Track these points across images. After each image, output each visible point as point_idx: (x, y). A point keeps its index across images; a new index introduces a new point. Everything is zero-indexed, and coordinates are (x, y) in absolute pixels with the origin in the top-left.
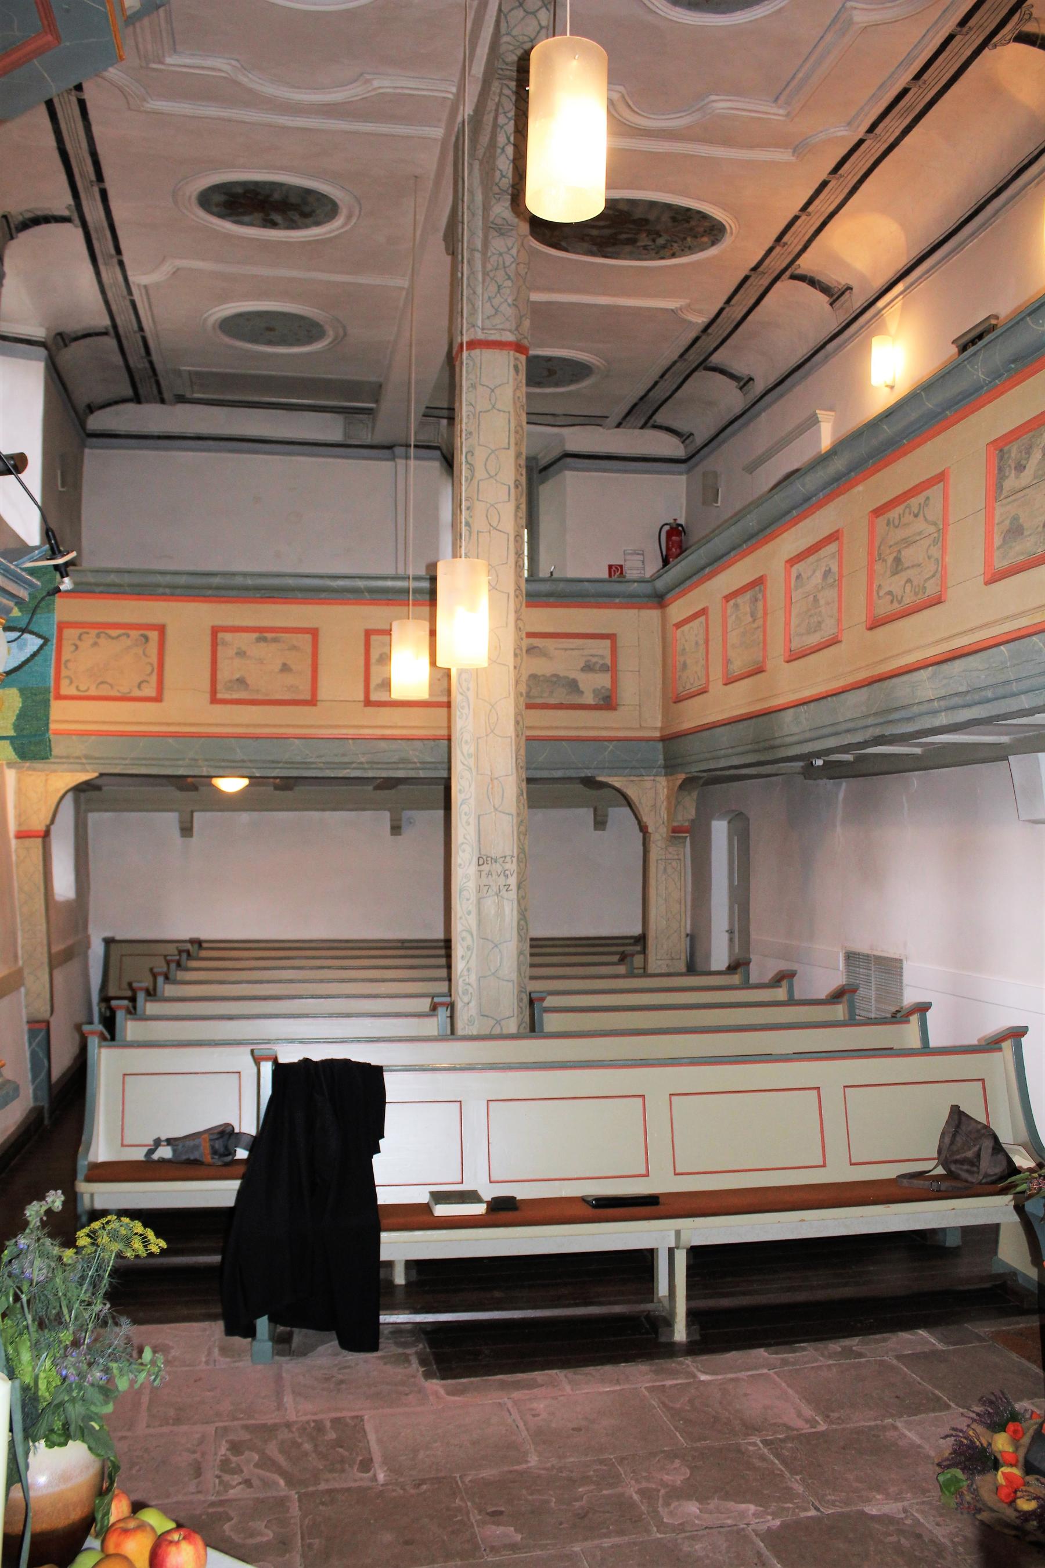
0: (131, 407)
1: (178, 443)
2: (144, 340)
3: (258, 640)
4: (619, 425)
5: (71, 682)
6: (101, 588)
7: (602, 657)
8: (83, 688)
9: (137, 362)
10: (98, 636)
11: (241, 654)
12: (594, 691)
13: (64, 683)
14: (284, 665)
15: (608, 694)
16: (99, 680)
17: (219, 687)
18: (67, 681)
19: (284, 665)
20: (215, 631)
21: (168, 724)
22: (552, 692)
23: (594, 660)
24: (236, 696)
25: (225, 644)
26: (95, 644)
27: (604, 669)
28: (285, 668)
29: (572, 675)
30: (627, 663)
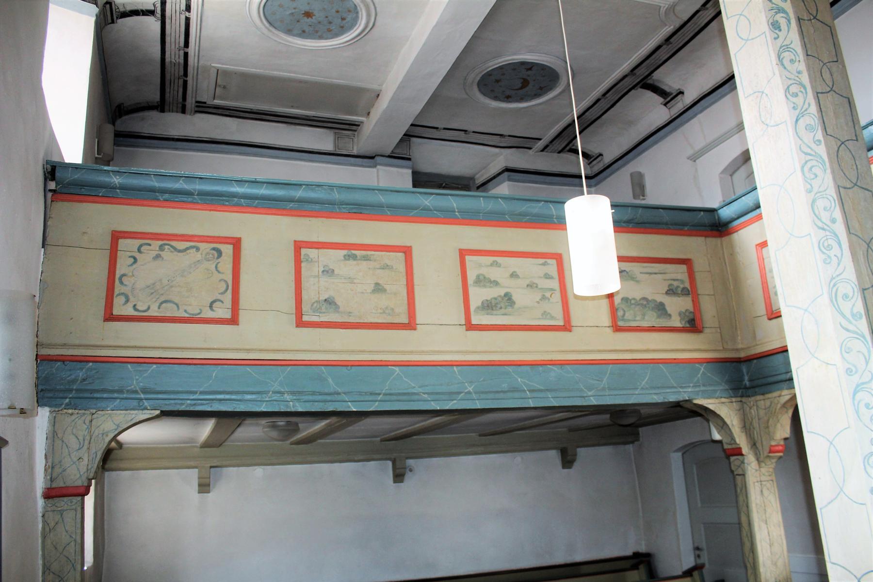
0: (154, 114)
2: (188, 20)
3: (347, 257)
5: (127, 301)
6: (166, 196)
7: (682, 282)
9: (173, 55)
10: (161, 248)
11: (328, 272)
12: (680, 314)
13: (118, 301)
14: (377, 284)
15: (691, 316)
16: (162, 299)
17: (305, 308)
18: (122, 299)
19: (377, 284)
21: (248, 351)
22: (644, 315)
23: (675, 283)
24: (324, 318)
25: (310, 261)
26: (158, 257)
27: (685, 292)
28: (378, 289)
29: (660, 298)
30: (704, 287)
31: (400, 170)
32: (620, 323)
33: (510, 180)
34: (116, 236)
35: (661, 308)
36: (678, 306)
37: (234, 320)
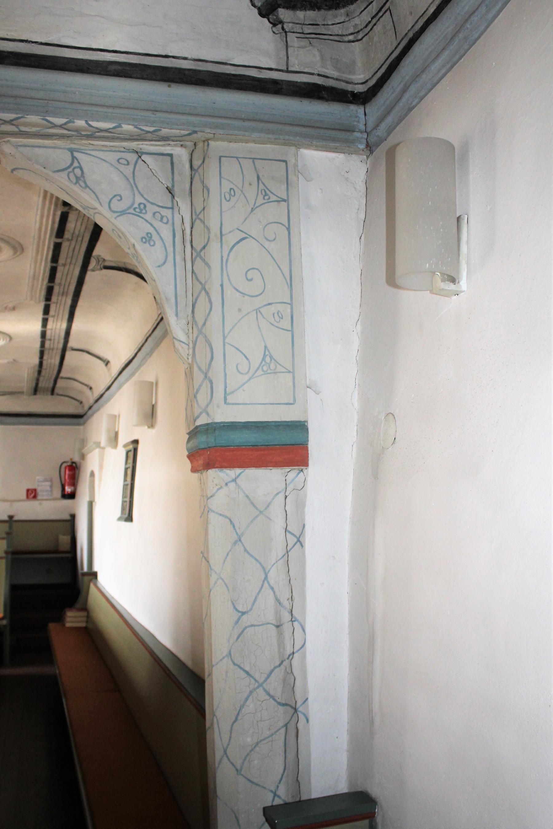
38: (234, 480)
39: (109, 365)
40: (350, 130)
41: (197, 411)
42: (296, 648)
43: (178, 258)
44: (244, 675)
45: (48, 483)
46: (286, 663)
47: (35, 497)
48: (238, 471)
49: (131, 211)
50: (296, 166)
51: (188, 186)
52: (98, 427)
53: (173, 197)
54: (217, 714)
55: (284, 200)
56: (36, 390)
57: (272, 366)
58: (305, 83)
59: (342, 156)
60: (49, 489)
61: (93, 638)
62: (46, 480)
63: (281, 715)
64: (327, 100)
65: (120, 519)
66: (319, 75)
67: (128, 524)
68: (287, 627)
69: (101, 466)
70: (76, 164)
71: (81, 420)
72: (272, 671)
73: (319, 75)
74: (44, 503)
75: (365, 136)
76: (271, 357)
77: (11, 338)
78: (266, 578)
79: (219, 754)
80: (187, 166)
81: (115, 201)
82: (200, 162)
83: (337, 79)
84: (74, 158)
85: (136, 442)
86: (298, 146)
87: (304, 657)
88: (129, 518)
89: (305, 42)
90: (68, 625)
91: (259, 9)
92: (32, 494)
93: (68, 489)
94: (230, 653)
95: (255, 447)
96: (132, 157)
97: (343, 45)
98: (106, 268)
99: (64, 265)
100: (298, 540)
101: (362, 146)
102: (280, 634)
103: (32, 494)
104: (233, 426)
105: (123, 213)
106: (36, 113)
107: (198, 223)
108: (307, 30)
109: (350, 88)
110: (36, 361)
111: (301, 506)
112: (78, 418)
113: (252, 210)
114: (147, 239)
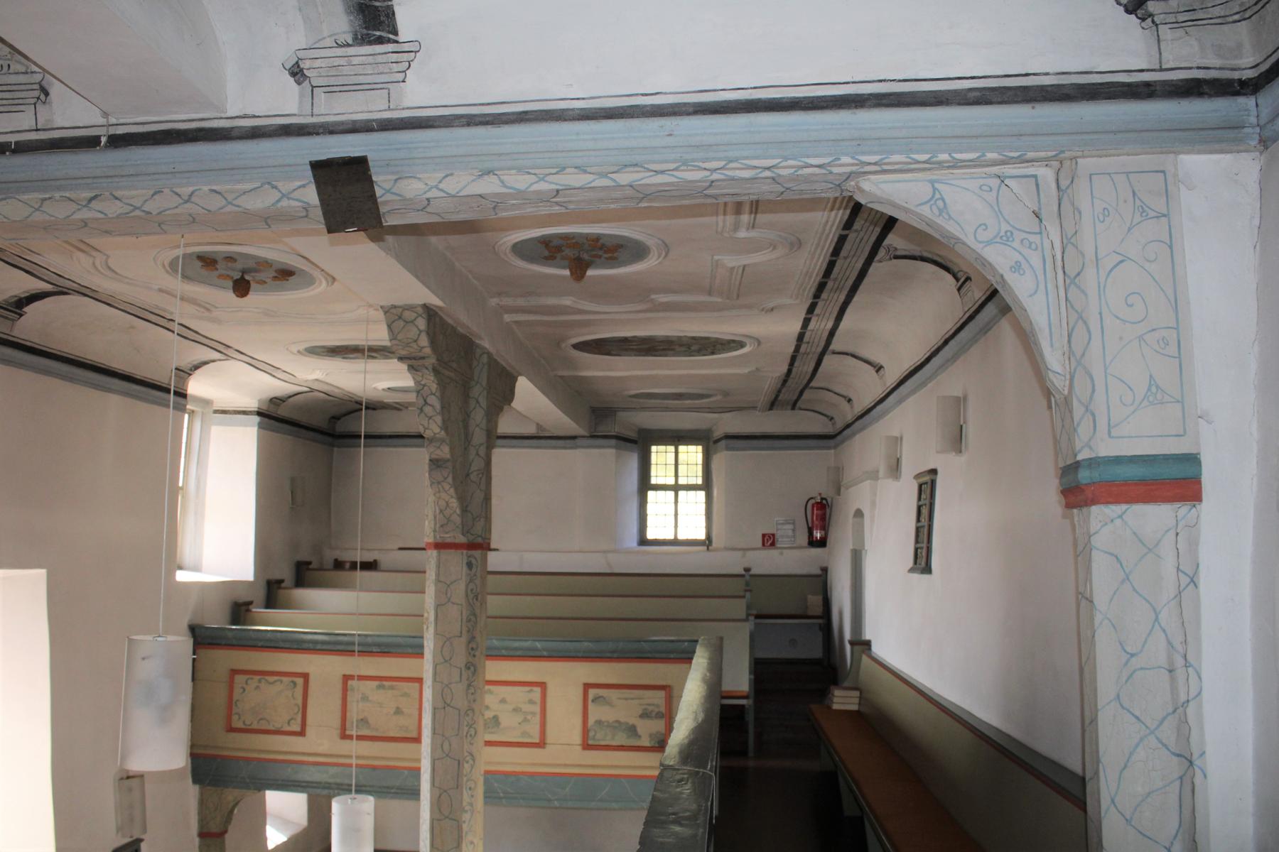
1: (379, 441)
3: (379, 687)
4: (771, 408)
7: (658, 706)
8: (248, 722)
10: (260, 681)
11: (365, 698)
12: (651, 735)
13: (235, 718)
20: (346, 678)
23: (651, 708)
26: (257, 687)
27: (659, 716)
28: (398, 711)
29: (632, 721)
31: (602, 451)
32: (590, 742)
33: (728, 448)
34: (234, 672)
35: (632, 731)
36: (646, 729)
37: (302, 733)
38: (1120, 517)
39: (882, 372)
40: (1238, 127)
41: (1078, 445)
42: (1191, 696)
43: (1049, 286)
44: (1134, 720)
45: (791, 527)
46: (1180, 710)
47: (773, 544)
48: (1124, 507)
49: (998, 240)
50: (1176, 175)
51: (1055, 208)
52: (868, 448)
53: (1041, 220)
54: (1103, 760)
55: (1164, 216)
56: (772, 405)
57: (1159, 396)
58: (1182, 80)
59: (1229, 156)
60: (792, 533)
61: (876, 725)
62: (787, 522)
63: (1175, 767)
64: (1210, 96)
65: (911, 570)
66: (1199, 68)
67: (926, 576)
68: (1180, 673)
69: (873, 504)
70: (937, 196)
71: (832, 442)
72: (1164, 719)
73: (1199, 68)
74: (785, 551)
75: (1258, 130)
76: (1157, 387)
77: (759, 343)
78: (1157, 619)
79: (1105, 803)
80: (1054, 185)
81: (980, 231)
82: (1068, 182)
83: (1220, 69)
84: (935, 189)
85: (934, 472)
86: (1177, 153)
87: (1200, 706)
88: (927, 569)
89: (1180, 32)
90: (835, 707)
91: (1125, 6)
92: (769, 541)
93: (818, 535)
94: (1118, 696)
95: (1143, 482)
96: (995, 182)
97: (1225, 27)
98: (896, 257)
99: (845, 258)
100: (1192, 581)
101: (1254, 143)
102: (1173, 680)
103: (769, 541)
104: (1118, 460)
105: (989, 243)
106: (900, 153)
107: (1070, 248)
108: (1181, 18)
109: (1236, 75)
110: (785, 368)
111: (1194, 544)
112: (831, 438)
113: (1129, 230)
114: (1017, 268)
